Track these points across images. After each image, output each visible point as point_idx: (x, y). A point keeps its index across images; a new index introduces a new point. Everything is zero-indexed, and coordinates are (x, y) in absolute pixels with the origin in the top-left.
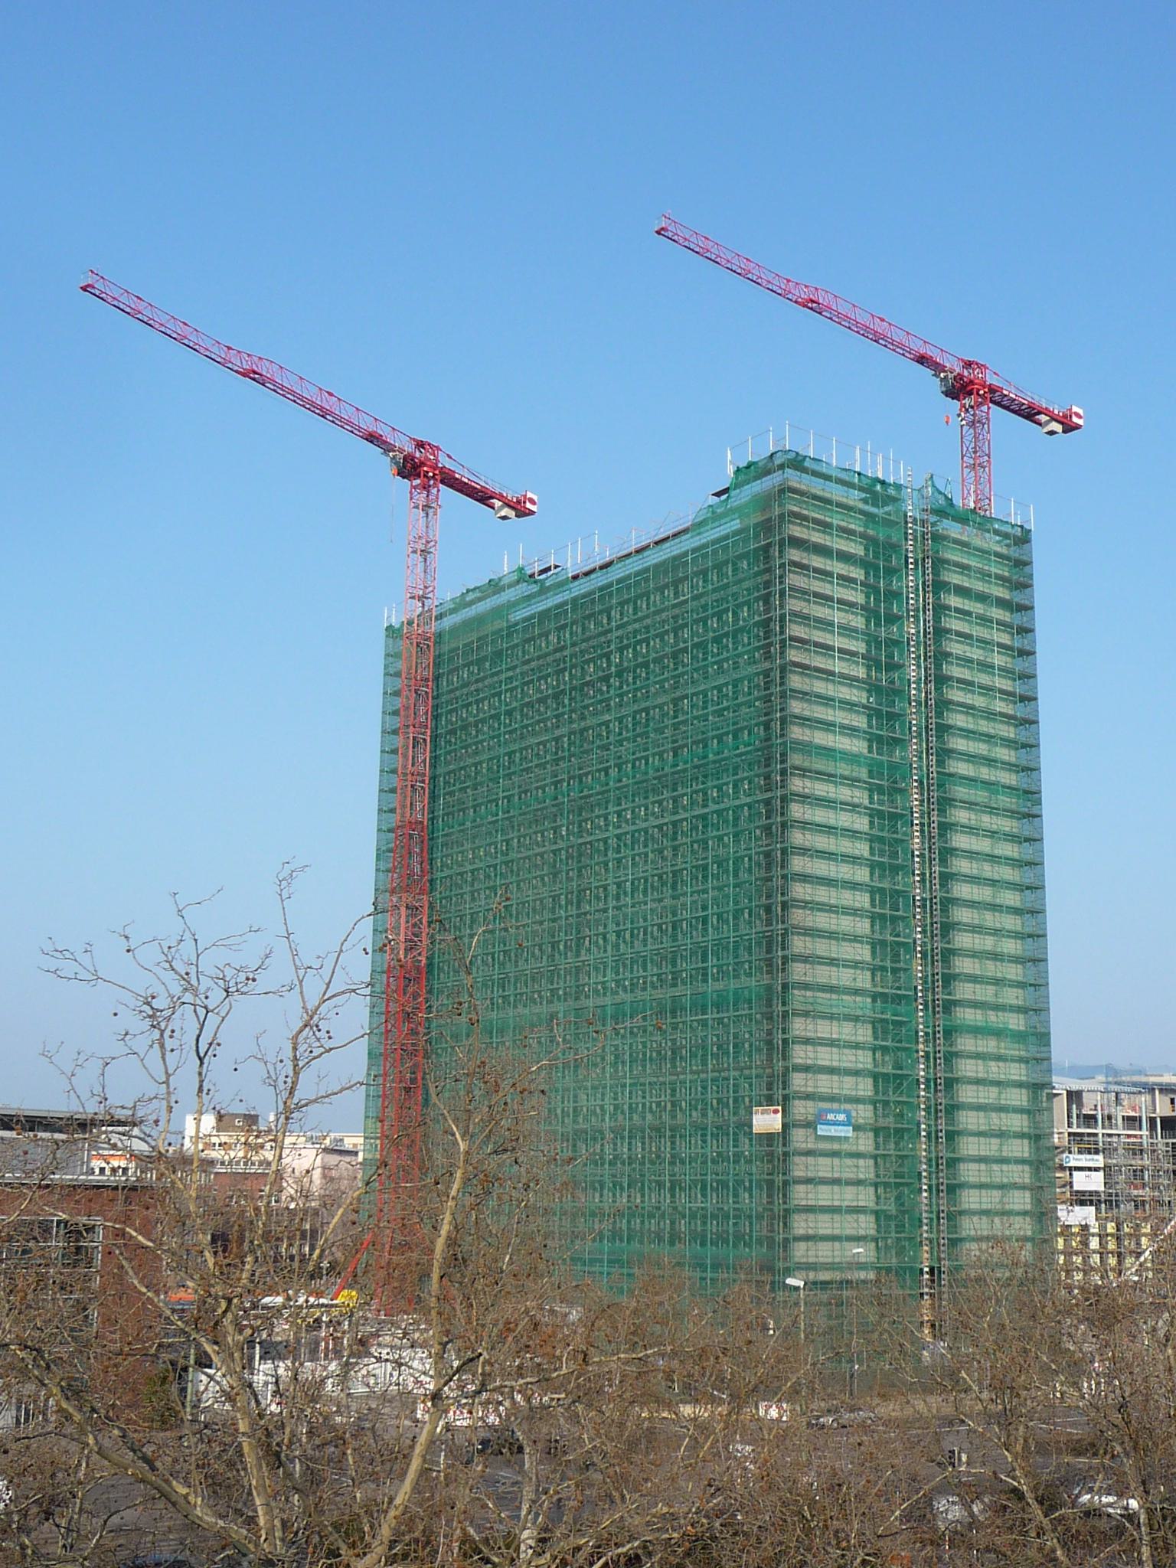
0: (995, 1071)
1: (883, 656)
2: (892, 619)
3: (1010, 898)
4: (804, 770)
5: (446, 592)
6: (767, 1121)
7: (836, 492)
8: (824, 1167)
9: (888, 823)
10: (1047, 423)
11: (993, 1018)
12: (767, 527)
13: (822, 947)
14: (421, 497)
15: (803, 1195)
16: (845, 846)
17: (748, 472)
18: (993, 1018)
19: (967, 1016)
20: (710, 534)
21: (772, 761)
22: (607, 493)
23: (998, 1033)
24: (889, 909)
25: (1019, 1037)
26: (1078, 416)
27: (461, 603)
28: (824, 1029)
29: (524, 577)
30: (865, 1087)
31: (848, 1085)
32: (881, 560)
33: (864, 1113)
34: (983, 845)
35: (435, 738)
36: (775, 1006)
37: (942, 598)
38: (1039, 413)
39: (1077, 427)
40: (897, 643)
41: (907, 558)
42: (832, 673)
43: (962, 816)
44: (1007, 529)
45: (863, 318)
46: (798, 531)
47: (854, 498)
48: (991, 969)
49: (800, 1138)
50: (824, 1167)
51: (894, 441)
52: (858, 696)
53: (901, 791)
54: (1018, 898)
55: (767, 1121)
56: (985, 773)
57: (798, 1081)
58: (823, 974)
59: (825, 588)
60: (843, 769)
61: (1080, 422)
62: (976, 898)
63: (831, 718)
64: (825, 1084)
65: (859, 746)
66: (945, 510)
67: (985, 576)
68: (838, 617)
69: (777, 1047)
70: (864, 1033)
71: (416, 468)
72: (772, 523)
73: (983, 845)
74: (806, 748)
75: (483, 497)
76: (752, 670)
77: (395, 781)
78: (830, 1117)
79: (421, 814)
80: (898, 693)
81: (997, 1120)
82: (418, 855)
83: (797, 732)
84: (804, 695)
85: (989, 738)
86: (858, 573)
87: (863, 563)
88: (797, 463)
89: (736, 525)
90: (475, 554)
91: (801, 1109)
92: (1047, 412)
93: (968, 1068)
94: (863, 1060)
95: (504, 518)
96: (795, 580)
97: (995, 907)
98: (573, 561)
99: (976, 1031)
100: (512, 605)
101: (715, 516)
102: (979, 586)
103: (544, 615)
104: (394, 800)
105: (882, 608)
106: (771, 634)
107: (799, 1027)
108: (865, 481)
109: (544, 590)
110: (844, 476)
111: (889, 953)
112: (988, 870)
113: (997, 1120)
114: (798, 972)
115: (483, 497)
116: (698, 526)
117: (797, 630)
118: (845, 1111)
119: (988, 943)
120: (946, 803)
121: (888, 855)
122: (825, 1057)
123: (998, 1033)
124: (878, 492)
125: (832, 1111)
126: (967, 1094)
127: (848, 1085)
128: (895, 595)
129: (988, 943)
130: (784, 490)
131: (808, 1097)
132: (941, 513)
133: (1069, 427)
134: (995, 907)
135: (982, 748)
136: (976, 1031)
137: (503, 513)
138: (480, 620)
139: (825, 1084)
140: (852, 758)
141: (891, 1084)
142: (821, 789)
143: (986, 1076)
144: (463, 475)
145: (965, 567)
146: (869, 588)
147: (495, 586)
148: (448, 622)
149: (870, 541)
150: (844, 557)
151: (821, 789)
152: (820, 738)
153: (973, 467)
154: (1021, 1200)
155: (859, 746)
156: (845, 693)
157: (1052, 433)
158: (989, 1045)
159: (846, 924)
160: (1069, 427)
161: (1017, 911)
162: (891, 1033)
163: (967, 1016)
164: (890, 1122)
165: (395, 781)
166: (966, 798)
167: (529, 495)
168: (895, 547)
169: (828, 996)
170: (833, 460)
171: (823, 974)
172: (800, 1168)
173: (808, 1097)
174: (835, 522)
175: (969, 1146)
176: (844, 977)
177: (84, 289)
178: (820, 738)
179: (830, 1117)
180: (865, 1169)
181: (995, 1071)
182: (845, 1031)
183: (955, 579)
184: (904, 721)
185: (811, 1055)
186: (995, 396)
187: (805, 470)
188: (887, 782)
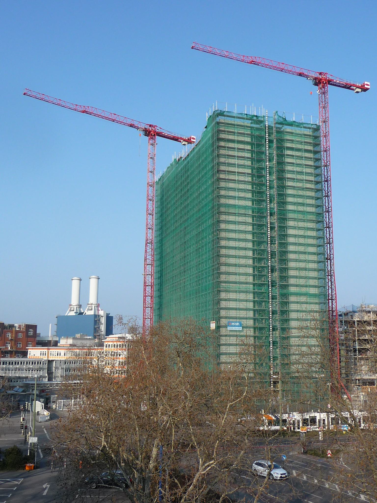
1: (258, 174)
4: (225, 213)
9: (258, 226)
10: (356, 89)
13: (232, 269)
14: (151, 142)
15: (224, 349)
19: (292, 289)
24: (259, 256)
26: (367, 85)
28: (232, 296)
32: (257, 142)
38: (351, 86)
39: (367, 89)
40: (263, 169)
41: (266, 140)
42: (235, 180)
44: (310, 126)
45: (275, 64)
47: (247, 123)
53: (264, 217)
54: (315, 249)
57: (223, 313)
58: (232, 278)
59: (231, 153)
61: (369, 87)
62: (297, 250)
64: (233, 313)
66: (284, 122)
71: (151, 133)
78: (233, 324)
80: (263, 185)
87: (251, 144)
92: (354, 85)
94: (316, 307)
95: (184, 145)
99: (296, 294)
105: (257, 157)
108: (249, 116)
110: (240, 116)
114: (223, 278)
118: (239, 322)
122: (232, 305)
125: (233, 322)
128: (262, 153)
131: (226, 318)
133: (364, 90)
136: (296, 294)
137: (183, 143)
139: (233, 313)
140: (245, 207)
142: (232, 218)
145: (292, 141)
149: (252, 136)
151: (232, 218)
152: (231, 202)
153: (324, 107)
157: (357, 92)
160: (364, 90)
163: (292, 289)
166: (293, 217)
167: (192, 137)
169: (235, 285)
170: (235, 111)
172: (223, 340)
173: (226, 318)
174: (236, 131)
177: (24, 94)
178: (231, 202)
179: (233, 324)
184: (265, 194)
185: (228, 304)
186: (329, 82)
187: (224, 116)
188: (259, 215)
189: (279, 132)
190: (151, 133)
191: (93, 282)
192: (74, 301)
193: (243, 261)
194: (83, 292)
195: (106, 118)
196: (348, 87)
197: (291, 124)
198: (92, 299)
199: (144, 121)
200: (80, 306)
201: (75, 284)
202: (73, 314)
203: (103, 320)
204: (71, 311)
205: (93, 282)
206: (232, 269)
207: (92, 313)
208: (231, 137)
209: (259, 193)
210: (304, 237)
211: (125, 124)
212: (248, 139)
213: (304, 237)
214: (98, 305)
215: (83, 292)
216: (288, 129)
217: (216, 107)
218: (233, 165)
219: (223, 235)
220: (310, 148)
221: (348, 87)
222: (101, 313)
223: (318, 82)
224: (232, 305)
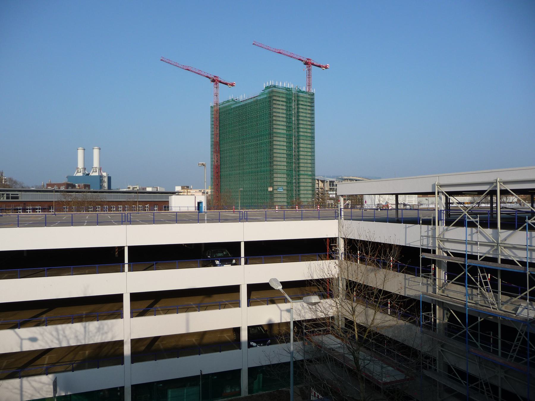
0: (306, 180)
2: (290, 110)
3: (309, 154)
5: (221, 101)
6: (270, 189)
7: (281, 91)
8: (279, 196)
11: (306, 173)
12: (270, 97)
13: (279, 163)
16: (282, 148)
17: (267, 88)
18: (306, 173)
19: (302, 172)
20: (262, 97)
21: (271, 135)
22: (245, 90)
23: (307, 175)
24: (289, 156)
25: (310, 175)
27: (223, 103)
28: (279, 175)
29: (233, 100)
30: (285, 184)
31: (282, 184)
32: (289, 101)
33: (285, 188)
34: (305, 146)
35: (220, 127)
36: (271, 172)
37: (299, 105)
43: (301, 130)
46: (275, 98)
47: (284, 91)
48: (306, 165)
49: (275, 192)
50: (279, 196)
51: (291, 79)
52: (285, 124)
55: (270, 189)
56: (306, 134)
57: (275, 183)
58: (279, 167)
60: (281, 95)
63: (280, 127)
64: (279, 184)
65: (285, 132)
66: (300, 91)
67: (306, 102)
68: (281, 115)
69: (272, 178)
70: (285, 176)
71: (215, 80)
72: (271, 94)
73: (305, 146)
74: (275, 133)
75: (226, 84)
76: (267, 140)
77: (213, 123)
79: (218, 140)
81: (306, 188)
82: (217, 147)
83: (275, 130)
84: (275, 112)
85: (306, 113)
86: (285, 104)
87: (286, 102)
88: (275, 87)
89: (265, 96)
90: (226, 95)
91: (275, 187)
93: (302, 180)
96: (275, 106)
97: (306, 132)
98: (241, 98)
99: (303, 175)
100: (231, 105)
101: (262, 94)
102: (305, 103)
103: (237, 107)
104: (213, 120)
106: (271, 115)
107: (275, 175)
109: (236, 103)
111: (289, 163)
112: (306, 150)
113: (306, 188)
114: (275, 167)
115: (226, 84)
116: (260, 96)
117: (275, 114)
119: (305, 161)
120: (298, 140)
121: (289, 148)
122: (279, 180)
123: (307, 175)
124: (288, 89)
126: (302, 184)
127: (282, 184)
129: (305, 161)
130: (272, 91)
132: (299, 92)
134: (306, 132)
135: (305, 130)
136: (303, 175)
138: (226, 107)
139: (279, 184)
140: (283, 134)
141: (289, 183)
143: (305, 183)
144: (223, 81)
146: (286, 106)
147: (228, 101)
148: (221, 106)
150: (282, 101)
154: (310, 185)
155: (285, 132)
156: (282, 123)
158: (306, 177)
159: (282, 151)
160: (326, 68)
161: (310, 129)
162: (289, 175)
163: (302, 172)
164: (289, 189)
165: (213, 120)
168: (291, 99)
171: (279, 167)
172: (275, 196)
175: (302, 192)
176: (282, 167)
180: (285, 196)
181: (306, 180)
182: (282, 176)
183: (301, 103)
188: (289, 137)
189: (298, 96)
190: (215, 80)
191: (96, 152)
192: (80, 165)
193: (282, 159)
194: (88, 159)
195: (197, 73)
196: (319, 66)
197: (303, 92)
198: (96, 164)
199: (212, 74)
200: (85, 169)
201: (80, 153)
202: (80, 174)
203: (106, 180)
204: (78, 172)
205: (96, 152)
206: (279, 163)
207: (96, 174)
208: (278, 99)
209: (290, 126)
210: (306, 148)
211: (204, 76)
212: (284, 100)
213: (306, 148)
214: (100, 169)
215: (88, 159)
216: (301, 94)
217: (271, 83)
218: (279, 113)
219: (275, 147)
220: (309, 104)
221: (319, 66)
222: (104, 174)
223: (306, 63)
224: (279, 180)
